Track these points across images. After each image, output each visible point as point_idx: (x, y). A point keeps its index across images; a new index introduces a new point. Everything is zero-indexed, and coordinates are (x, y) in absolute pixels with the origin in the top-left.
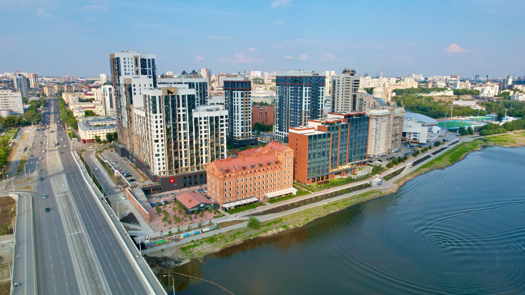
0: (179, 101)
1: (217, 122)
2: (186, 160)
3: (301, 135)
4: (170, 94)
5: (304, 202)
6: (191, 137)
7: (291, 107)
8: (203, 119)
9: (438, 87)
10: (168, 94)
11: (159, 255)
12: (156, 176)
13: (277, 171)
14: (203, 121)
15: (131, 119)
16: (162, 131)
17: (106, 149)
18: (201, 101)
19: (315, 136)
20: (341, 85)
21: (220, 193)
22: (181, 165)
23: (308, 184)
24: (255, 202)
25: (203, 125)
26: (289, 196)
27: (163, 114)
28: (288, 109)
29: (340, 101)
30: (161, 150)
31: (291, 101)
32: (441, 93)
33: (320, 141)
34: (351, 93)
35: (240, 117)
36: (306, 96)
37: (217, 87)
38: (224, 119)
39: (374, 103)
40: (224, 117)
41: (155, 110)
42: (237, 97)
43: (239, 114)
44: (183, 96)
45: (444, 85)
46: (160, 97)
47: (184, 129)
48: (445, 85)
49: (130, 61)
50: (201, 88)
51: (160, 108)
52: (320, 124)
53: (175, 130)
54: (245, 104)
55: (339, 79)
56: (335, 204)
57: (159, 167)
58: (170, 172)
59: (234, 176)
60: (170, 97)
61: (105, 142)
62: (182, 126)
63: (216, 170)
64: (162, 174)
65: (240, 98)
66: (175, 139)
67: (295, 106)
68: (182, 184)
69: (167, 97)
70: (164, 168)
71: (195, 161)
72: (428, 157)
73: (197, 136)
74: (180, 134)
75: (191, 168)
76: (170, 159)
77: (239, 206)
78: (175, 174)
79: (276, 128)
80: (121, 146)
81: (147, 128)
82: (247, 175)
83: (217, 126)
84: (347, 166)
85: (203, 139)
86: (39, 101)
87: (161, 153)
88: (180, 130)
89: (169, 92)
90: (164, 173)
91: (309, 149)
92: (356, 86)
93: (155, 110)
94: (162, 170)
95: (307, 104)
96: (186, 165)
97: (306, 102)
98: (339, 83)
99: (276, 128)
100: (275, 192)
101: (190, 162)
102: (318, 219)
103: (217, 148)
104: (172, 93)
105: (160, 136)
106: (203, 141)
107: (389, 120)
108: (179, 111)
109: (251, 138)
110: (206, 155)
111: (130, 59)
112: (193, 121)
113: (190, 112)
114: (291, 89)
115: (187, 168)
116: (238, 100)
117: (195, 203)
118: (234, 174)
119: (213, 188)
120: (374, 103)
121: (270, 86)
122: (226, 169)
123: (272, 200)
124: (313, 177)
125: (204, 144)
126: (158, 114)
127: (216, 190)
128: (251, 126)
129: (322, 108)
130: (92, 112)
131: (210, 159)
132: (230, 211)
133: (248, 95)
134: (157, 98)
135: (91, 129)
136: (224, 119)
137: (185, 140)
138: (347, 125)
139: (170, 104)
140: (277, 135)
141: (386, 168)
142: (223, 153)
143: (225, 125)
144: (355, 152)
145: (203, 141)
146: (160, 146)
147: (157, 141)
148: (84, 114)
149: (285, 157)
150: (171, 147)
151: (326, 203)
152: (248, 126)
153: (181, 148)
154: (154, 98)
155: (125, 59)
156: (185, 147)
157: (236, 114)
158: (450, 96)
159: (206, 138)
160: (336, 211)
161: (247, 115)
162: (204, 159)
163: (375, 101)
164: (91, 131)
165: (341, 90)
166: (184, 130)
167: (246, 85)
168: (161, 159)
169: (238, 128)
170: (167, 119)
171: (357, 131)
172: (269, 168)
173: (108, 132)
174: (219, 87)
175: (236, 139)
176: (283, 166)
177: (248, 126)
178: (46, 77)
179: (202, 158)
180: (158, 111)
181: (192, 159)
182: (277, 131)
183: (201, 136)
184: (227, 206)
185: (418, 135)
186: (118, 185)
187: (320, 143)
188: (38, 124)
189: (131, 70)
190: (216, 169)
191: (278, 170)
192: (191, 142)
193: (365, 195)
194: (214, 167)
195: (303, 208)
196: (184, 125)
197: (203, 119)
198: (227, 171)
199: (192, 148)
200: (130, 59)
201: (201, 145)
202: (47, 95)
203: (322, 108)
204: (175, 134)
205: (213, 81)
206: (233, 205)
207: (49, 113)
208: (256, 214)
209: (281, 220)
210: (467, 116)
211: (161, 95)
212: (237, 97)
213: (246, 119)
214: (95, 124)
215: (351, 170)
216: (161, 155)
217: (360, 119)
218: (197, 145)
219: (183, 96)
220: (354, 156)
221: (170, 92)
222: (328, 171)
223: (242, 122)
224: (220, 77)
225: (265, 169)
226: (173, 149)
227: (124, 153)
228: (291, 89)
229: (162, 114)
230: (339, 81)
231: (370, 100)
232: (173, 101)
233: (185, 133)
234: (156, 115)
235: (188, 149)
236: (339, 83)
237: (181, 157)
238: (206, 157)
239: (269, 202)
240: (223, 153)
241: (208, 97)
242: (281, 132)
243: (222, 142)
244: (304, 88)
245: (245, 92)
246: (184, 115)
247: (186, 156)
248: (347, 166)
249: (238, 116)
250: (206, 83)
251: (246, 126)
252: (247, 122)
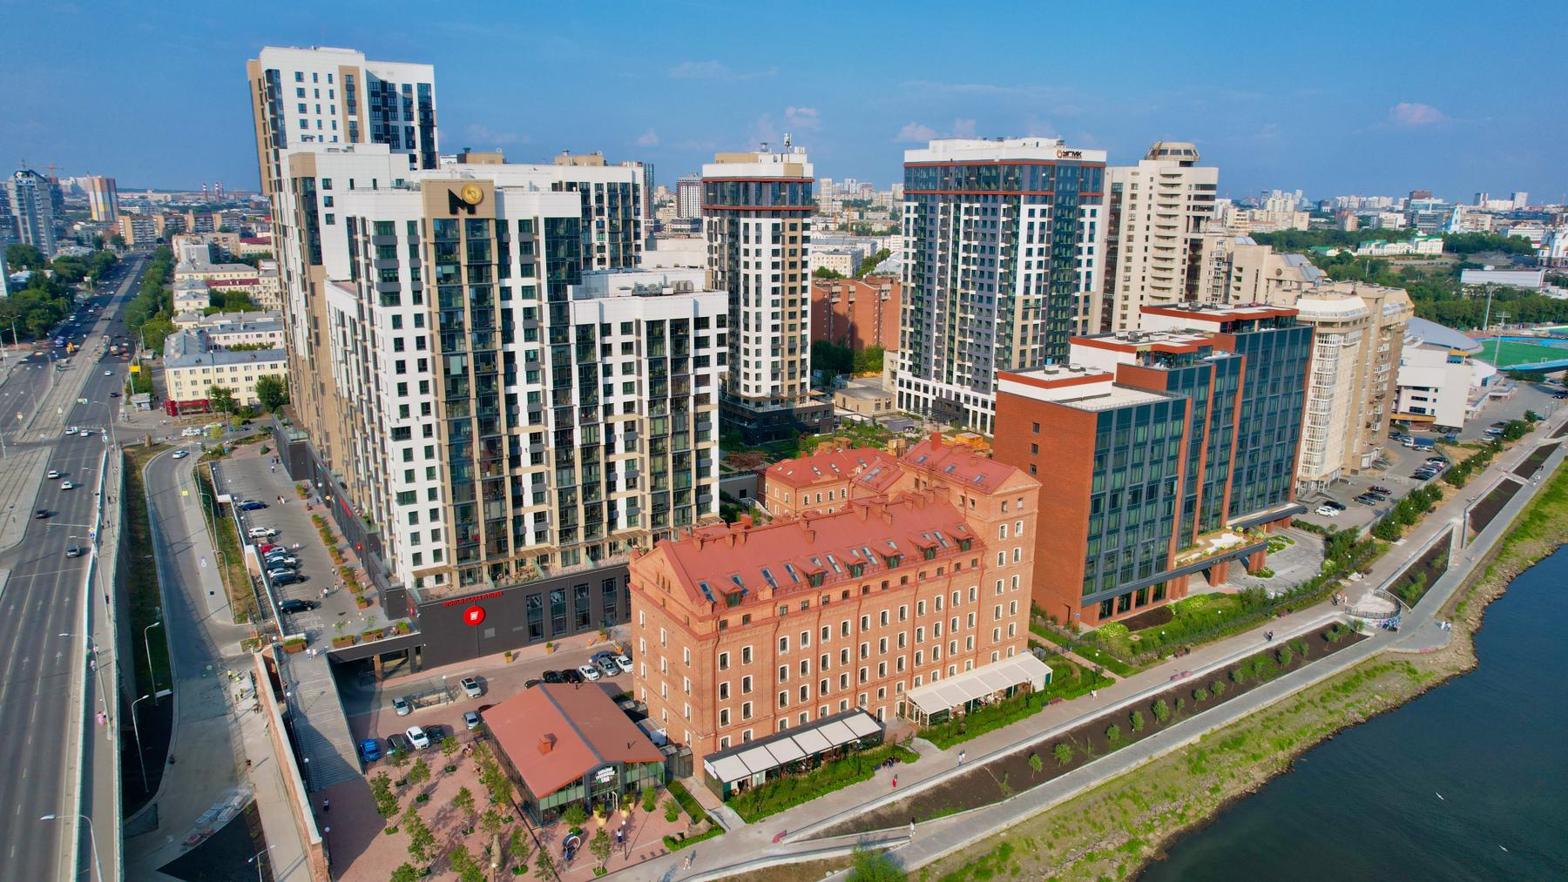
0: (504, 249)
1: (679, 343)
2: (539, 517)
3: (1057, 408)
4: (463, 214)
5: (1096, 739)
6: (563, 414)
7: (964, 284)
8: (616, 329)
9: (1385, 226)
10: (453, 211)
12: (401, 590)
14: (616, 339)
15: (316, 327)
16: (424, 387)
17: (248, 440)
18: (614, 260)
19: (1124, 413)
20: (1142, 202)
21: (694, 704)
22: (519, 540)
23: (1085, 628)
24: (869, 741)
25: (617, 359)
26: (1019, 701)
27: (430, 307)
28: (954, 291)
29: (1137, 264)
30: (420, 474)
31: (966, 260)
32: (1399, 248)
33: (1141, 434)
34: (1181, 234)
35: (767, 322)
36: (1030, 240)
37: (674, 222)
38: (712, 332)
39: (1279, 272)
40: (713, 322)
41: (390, 287)
42: (758, 239)
43: (762, 308)
44: (524, 225)
45: (1401, 220)
46: (412, 225)
47: (532, 377)
48: (1404, 222)
49: (323, 86)
50: (613, 209)
51: (416, 278)
52: (1130, 359)
53: (486, 380)
54: (788, 272)
55: (1136, 180)
56: (1234, 741)
57: (418, 548)
58: (467, 575)
59: (765, 622)
60: (462, 226)
61: (252, 411)
62: (520, 361)
63: (678, 589)
64: (429, 582)
65: (767, 245)
66: (487, 425)
67: (984, 280)
68: (521, 629)
69: (445, 226)
70: (437, 554)
71: (581, 521)
72: (1508, 489)
73: (588, 409)
74: (511, 400)
75: (565, 555)
76: (465, 514)
77: (792, 767)
78: (487, 584)
79: (896, 361)
80: (291, 435)
81: (367, 370)
82: (827, 613)
83: (679, 362)
84: (1226, 540)
85: (619, 421)
86: (85, 260)
87: (421, 486)
88: (510, 379)
89: (456, 203)
90: (439, 578)
91: (1096, 474)
92: (1202, 209)
93: (390, 287)
94: (428, 562)
95: (1034, 272)
96: (540, 536)
97: (1028, 266)
98: (1133, 196)
99: (896, 361)
100: (950, 682)
101: (556, 527)
102: (1178, 836)
103: (679, 459)
104: (471, 209)
105: (415, 410)
106: (619, 430)
107: (1365, 340)
108: (506, 293)
109: (809, 403)
110: (632, 493)
111: (323, 79)
112: (573, 339)
113: (557, 293)
114: (968, 211)
115: (544, 553)
116: (758, 253)
117: (573, 760)
118: (767, 612)
119: (659, 654)
120: (1279, 272)
121: (840, 221)
122: (728, 587)
123: (945, 728)
124: (1107, 594)
125: (620, 445)
126: (407, 308)
127: (675, 685)
128: (807, 356)
129: (1088, 287)
131: (648, 511)
132: (754, 800)
133: (798, 233)
134: (401, 233)
135: (199, 362)
136: (712, 332)
137: (536, 429)
138: (1235, 363)
139: (464, 260)
140: (905, 390)
141: (1378, 542)
142: (704, 481)
143: (713, 360)
144: (1250, 474)
145: (619, 430)
146: (419, 454)
147: (402, 433)
148: (206, 303)
149: (999, 516)
150: (470, 461)
151: (1195, 739)
152: (797, 358)
153: (515, 461)
154: (386, 228)
155: (299, 77)
156: (536, 458)
157: (752, 309)
158: (1432, 257)
159: (630, 417)
160: (1249, 786)
161: (792, 315)
162: (622, 507)
163: (1282, 266)
164: (199, 369)
165: (1140, 223)
166: (529, 381)
167: (794, 194)
168: (424, 516)
169: (758, 365)
170: (450, 334)
171: (1267, 389)
172: (931, 569)
173: (268, 371)
174: (681, 222)
175: (752, 406)
176: (990, 560)
177: (797, 358)
178: (156, 191)
179: (612, 506)
180: (406, 294)
181: (566, 512)
182: (906, 375)
183: (608, 409)
184: (730, 770)
185: (1430, 395)
186: (241, 618)
187: (1142, 445)
188: (44, 337)
189: (327, 125)
190: (676, 584)
191: (968, 577)
192: (563, 437)
194: (669, 572)
196: (531, 358)
197: (616, 329)
198: (735, 599)
199: (564, 464)
200: (323, 79)
201: (610, 448)
202: (130, 241)
203: (1088, 287)
204: (487, 400)
205: (662, 205)
206: (759, 761)
207: (105, 301)
208: (880, 821)
209: (1005, 849)
210: (1537, 322)
211: (418, 214)
212: (758, 239)
213: (792, 328)
214: (234, 340)
215: (1246, 558)
216: (422, 495)
217: (1281, 336)
218: (589, 450)
219: (524, 225)
220: (1247, 491)
221: (463, 204)
222: (1163, 560)
223: (775, 340)
224: (683, 189)
225: (911, 576)
226: (477, 467)
227: (301, 462)
228: (968, 211)
229: (423, 309)
230: (1133, 186)
231: (1261, 260)
232: (478, 251)
233: (533, 397)
234: (395, 310)
235: (549, 467)
236: (1133, 196)
237: (518, 501)
238: (632, 502)
239: (930, 736)
240: (704, 481)
241: (641, 242)
242: (922, 382)
243: (701, 435)
244: (1025, 209)
245: (789, 221)
246: (528, 313)
247: (538, 498)
248: (1226, 540)
249: (758, 316)
250: (636, 187)
251: (788, 358)
252: (792, 340)
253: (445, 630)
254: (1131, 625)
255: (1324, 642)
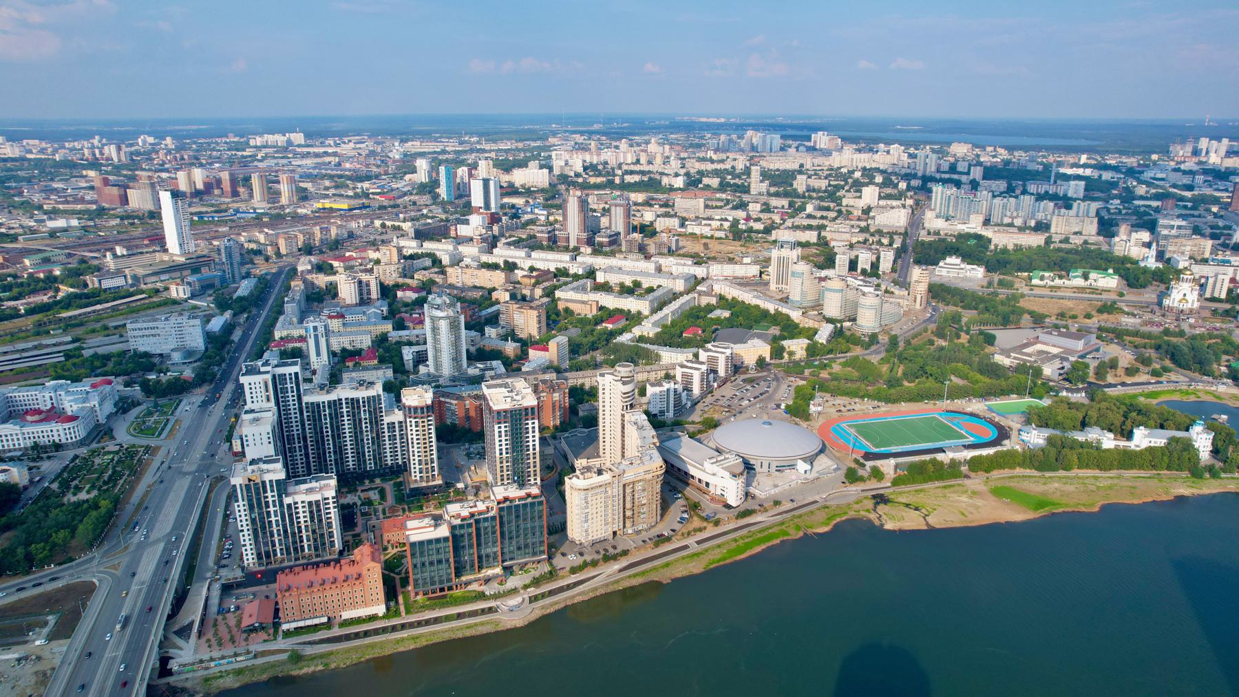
5: (394, 629)
11: (180, 685)
13: (358, 588)
14: (300, 505)
58: (260, 565)
72: (686, 547)
77: (301, 628)
89: (250, 480)
113: (280, 496)
130: (300, 349)
176: (367, 582)
193: (468, 627)
195: (368, 641)
206: (294, 625)
218: (294, 534)
253: (251, 579)
254: (429, 599)
255: (490, 610)
